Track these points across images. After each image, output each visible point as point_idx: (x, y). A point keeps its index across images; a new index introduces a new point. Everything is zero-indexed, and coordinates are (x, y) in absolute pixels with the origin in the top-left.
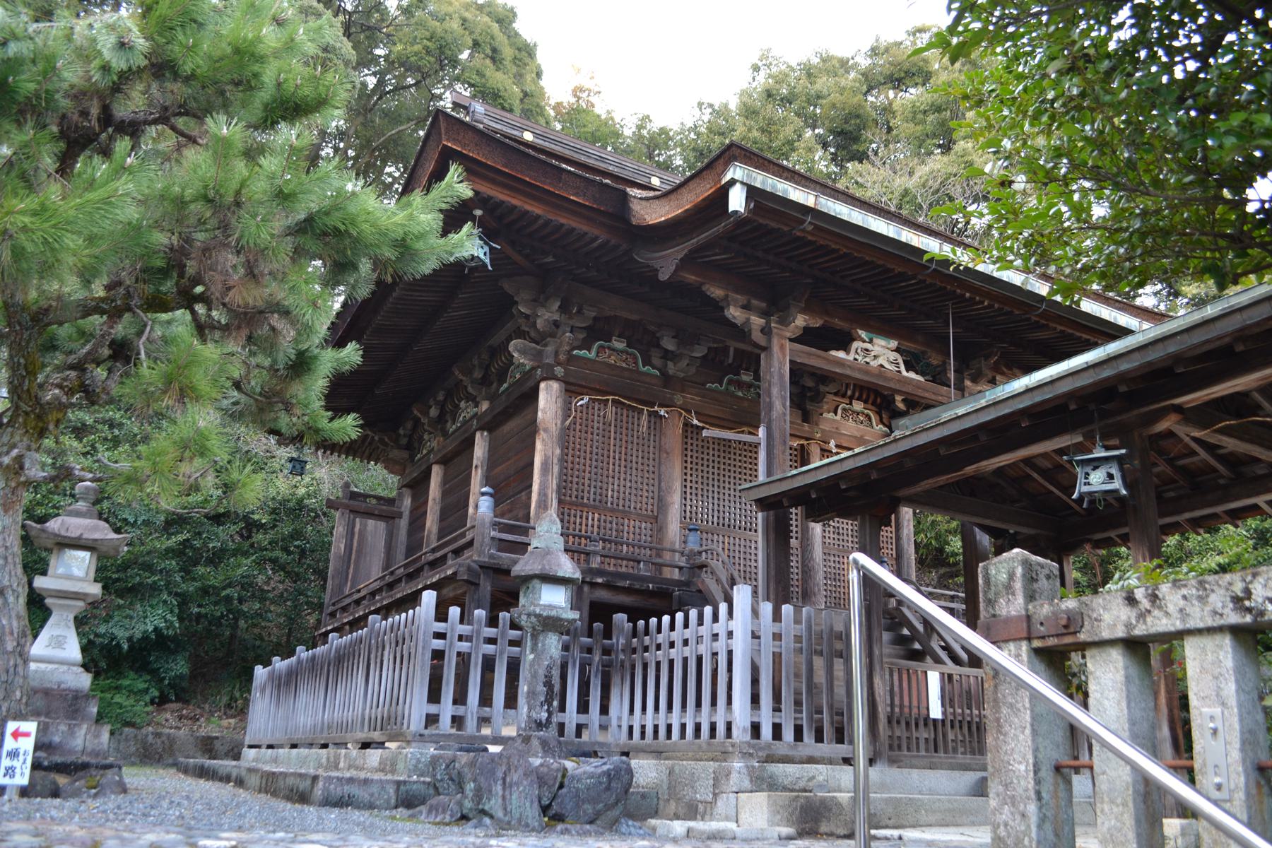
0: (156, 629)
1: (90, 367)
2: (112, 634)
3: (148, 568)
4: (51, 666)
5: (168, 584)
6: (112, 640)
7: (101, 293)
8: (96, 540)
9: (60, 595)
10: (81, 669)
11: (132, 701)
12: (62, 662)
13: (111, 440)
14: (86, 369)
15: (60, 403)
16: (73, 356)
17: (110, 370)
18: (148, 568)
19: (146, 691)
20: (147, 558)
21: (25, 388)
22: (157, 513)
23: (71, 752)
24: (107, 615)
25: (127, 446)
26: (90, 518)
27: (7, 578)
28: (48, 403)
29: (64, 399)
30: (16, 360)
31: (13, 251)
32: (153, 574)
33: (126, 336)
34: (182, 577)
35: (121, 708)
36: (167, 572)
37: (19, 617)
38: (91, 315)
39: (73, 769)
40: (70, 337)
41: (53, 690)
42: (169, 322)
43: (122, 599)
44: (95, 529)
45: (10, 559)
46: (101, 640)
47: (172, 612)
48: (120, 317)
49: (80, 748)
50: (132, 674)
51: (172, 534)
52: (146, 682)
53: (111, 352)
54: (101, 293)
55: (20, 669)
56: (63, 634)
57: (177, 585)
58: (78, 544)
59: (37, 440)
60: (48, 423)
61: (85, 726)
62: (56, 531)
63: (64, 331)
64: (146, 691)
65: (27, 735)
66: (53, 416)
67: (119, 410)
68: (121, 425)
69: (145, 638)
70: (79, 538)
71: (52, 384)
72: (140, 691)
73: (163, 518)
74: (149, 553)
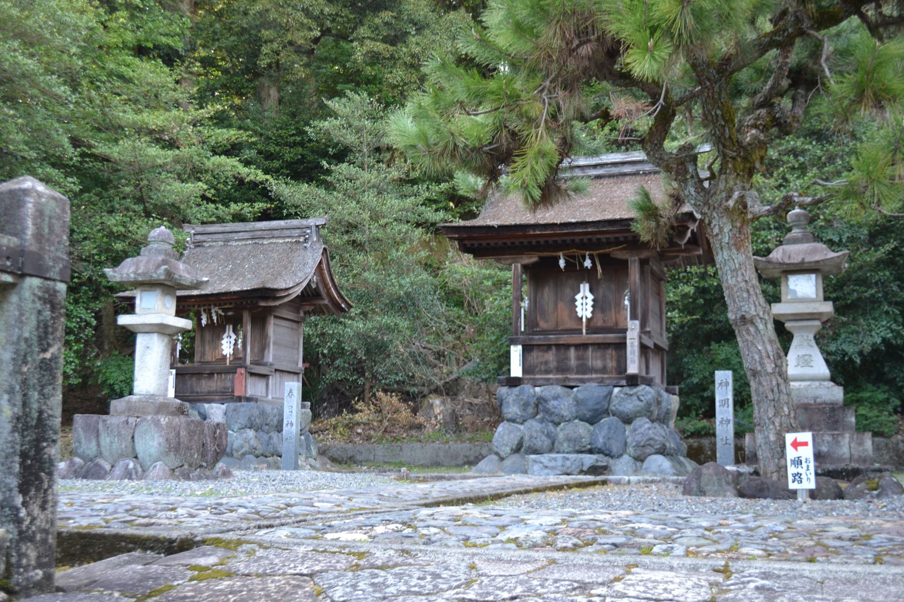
0: (884, 340)
1: (776, 100)
2: (843, 350)
3: (863, 282)
4: (804, 384)
5: (886, 294)
6: (844, 356)
7: (768, 27)
8: (818, 262)
9: (797, 318)
10: (832, 384)
11: (876, 412)
12: (813, 379)
13: (798, 168)
14: (773, 103)
15: (760, 141)
16: (759, 95)
17: (794, 99)
18: (863, 282)
19: (887, 401)
20: (860, 273)
21: (727, 136)
22: (860, 227)
23: (840, 459)
24: (834, 333)
25: (815, 170)
26: (808, 242)
27: (753, 308)
28: (749, 144)
29: (762, 137)
30: (713, 113)
31: (693, 14)
32: (869, 287)
33: (799, 61)
34: (898, 286)
35: (866, 419)
36: (883, 283)
37: (771, 342)
38: (767, 51)
39: (851, 474)
40: (751, 79)
41: (810, 404)
42: (838, 35)
43: (844, 315)
44: (814, 251)
45: (751, 290)
46: (833, 357)
47: (896, 321)
48: (792, 44)
49: (847, 456)
50: (870, 386)
51: (879, 245)
52: (885, 392)
53: (790, 81)
54: (768, 27)
55: (783, 387)
56: (807, 353)
57: (895, 294)
58: (801, 269)
59: (748, 181)
60: (754, 163)
61: (847, 435)
62: (780, 260)
63: (744, 75)
64: (887, 401)
65: (805, 444)
66: (756, 155)
67: (798, 138)
68: (803, 152)
69: (875, 350)
70: (803, 262)
71: (748, 126)
72: (881, 402)
73: (866, 232)
74: (861, 268)
